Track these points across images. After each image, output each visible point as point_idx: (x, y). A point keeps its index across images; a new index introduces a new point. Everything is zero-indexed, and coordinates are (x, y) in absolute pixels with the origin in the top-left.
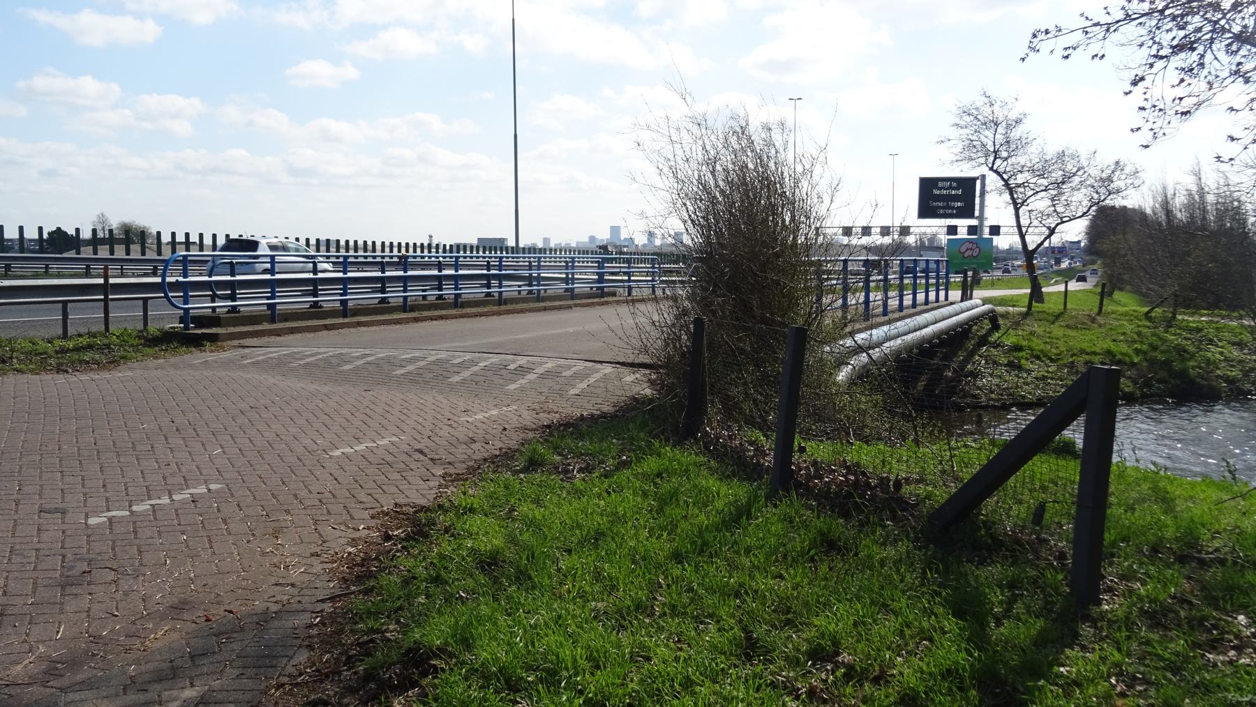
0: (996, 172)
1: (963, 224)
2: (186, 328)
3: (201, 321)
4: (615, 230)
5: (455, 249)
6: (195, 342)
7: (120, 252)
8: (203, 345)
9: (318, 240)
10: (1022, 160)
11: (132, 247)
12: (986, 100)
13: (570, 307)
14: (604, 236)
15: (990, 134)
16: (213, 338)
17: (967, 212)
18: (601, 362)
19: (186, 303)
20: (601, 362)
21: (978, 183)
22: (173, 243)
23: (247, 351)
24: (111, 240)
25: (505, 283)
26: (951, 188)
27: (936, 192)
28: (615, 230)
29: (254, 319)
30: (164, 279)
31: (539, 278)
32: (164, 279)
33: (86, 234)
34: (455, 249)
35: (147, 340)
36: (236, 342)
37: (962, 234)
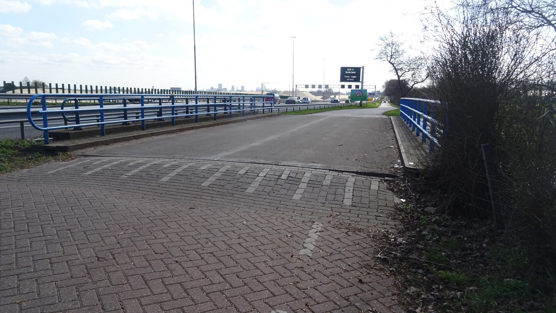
0: (391, 63)
1: (354, 84)
2: (46, 142)
3: (58, 136)
4: (220, 85)
5: (163, 92)
6: (53, 152)
7: (33, 92)
8: (57, 155)
9: (110, 87)
10: (401, 58)
11: (38, 90)
12: (391, 34)
13: (245, 120)
14: (216, 87)
15: (390, 48)
16: (64, 150)
17: (357, 80)
18: (342, 172)
19: (45, 125)
20: (342, 172)
21: (361, 69)
22: (57, 89)
23: (88, 160)
24: (29, 87)
25: (217, 108)
26: (352, 71)
27: (346, 72)
28: (220, 85)
29: (90, 133)
30: (28, 110)
31: (231, 106)
32: (28, 110)
33: (17, 84)
34: (163, 92)
35: (20, 150)
36: (79, 152)
37: (354, 88)
